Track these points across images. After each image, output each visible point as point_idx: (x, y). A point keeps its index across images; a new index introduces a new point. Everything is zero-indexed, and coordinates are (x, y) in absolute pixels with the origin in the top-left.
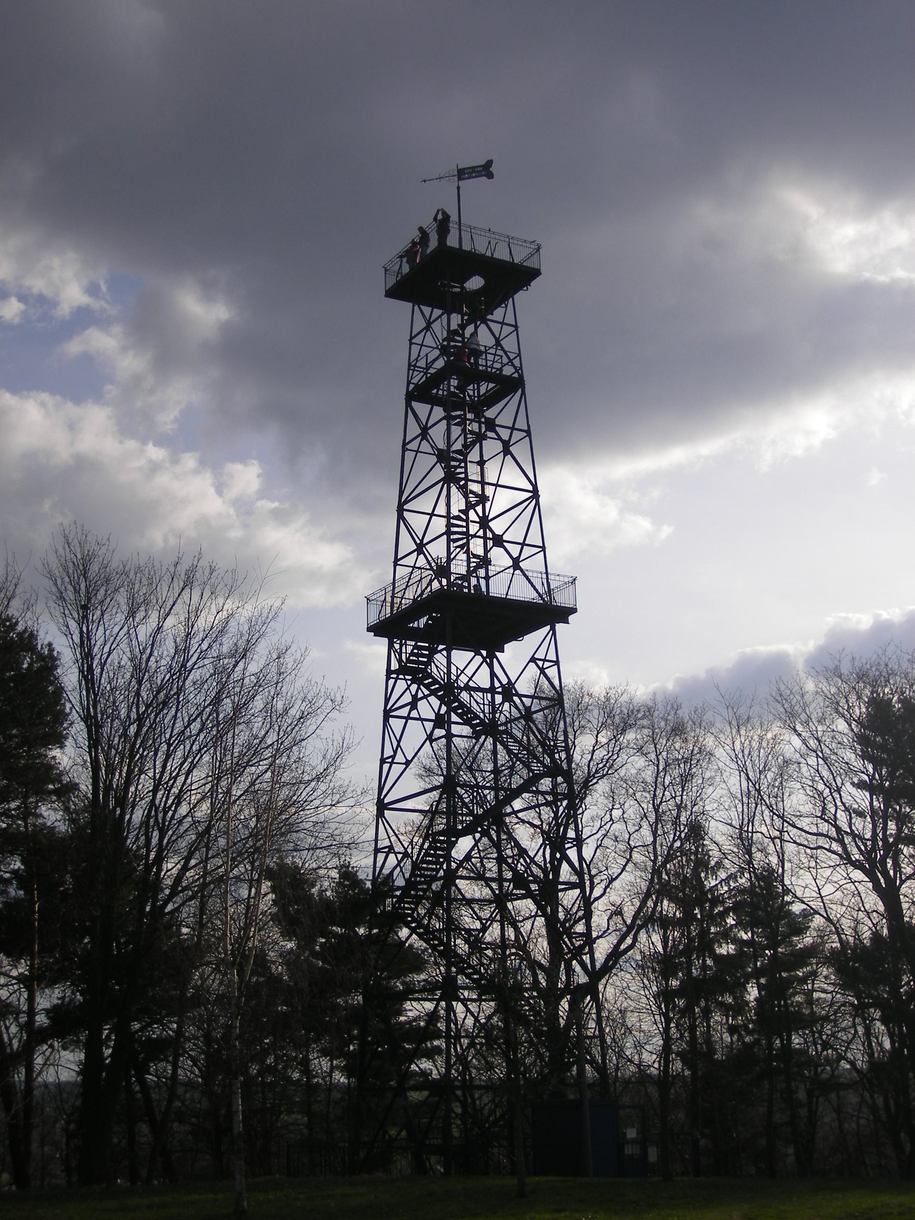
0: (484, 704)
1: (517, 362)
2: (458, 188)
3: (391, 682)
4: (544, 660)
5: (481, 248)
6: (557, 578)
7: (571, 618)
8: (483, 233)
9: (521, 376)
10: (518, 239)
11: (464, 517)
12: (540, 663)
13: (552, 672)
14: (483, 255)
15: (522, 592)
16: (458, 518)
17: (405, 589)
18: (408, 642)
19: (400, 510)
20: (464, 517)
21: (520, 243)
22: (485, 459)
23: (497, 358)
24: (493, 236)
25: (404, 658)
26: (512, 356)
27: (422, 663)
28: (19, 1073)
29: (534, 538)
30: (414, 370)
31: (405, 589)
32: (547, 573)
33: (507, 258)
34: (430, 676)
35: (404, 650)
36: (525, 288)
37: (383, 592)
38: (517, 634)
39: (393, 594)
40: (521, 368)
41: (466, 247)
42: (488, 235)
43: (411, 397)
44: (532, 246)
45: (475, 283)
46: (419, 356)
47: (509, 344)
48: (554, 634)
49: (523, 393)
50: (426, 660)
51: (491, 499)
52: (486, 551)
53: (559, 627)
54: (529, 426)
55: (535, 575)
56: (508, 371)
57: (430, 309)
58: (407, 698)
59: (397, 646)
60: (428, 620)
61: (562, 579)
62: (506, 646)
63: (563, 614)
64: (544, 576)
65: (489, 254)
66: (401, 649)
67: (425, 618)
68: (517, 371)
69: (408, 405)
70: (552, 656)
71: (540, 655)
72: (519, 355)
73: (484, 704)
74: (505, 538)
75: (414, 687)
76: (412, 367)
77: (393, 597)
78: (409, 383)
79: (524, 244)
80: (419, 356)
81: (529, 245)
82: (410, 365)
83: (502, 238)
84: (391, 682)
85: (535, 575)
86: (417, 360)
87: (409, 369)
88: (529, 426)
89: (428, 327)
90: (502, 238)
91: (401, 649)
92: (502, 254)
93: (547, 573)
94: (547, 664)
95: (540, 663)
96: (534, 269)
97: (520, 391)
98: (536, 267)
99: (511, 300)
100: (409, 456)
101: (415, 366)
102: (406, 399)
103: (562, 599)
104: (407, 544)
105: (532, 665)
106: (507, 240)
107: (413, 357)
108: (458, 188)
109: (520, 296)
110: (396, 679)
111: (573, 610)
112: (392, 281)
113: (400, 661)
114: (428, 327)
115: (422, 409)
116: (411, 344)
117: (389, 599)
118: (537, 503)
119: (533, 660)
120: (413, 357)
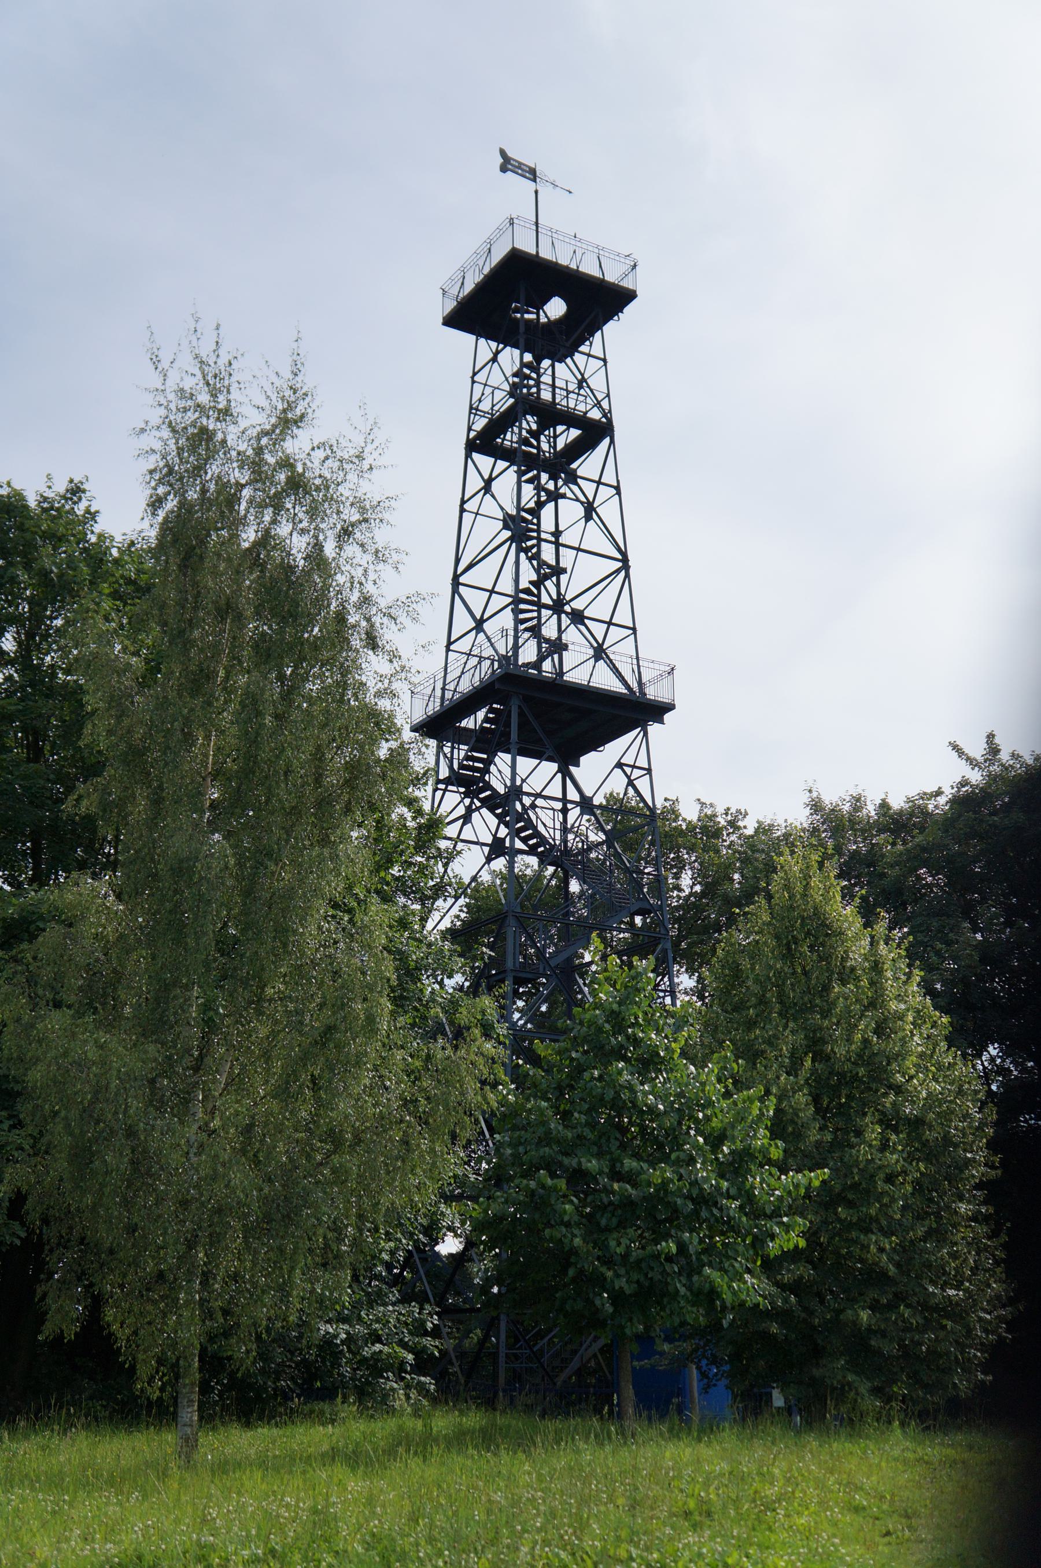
0: (554, 829)
1: (605, 404)
2: (536, 192)
3: (439, 794)
4: (633, 767)
5: (564, 259)
6: (651, 665)
7: (667, 717)
8: (567, 240)
9: (610, 421)
10: (611, 251)
11: (535, 591)
12: (628, 770)
13: (642, 784)
14: (567, 267)
15: (604, 680)
16: (527, 591)
17: (460, 677)
18: (461, 747)
19: (456, 582)
20: (535, 591)
21: (612, 256)
22: (561, 529)
23: (581, 398)
24: (579, 244)
25: (456, 766)
26: (600, 397)
27: (477, 770)
28: (684, 1285)
29: (623, 616)
30: (476, 414)
31: (460, 677)
32: (637, 658)
33: (595, 272)
34: (488, 786)
35: (456, 756)
36: (616, 318)
37: (432, 681)
38: (595, 743)
39: (445, 684)
40: (610, 411)
41: (546, 254)
42: (573, 242)
43: (472, 446)
44: (628, 262)
45: (556, 308)
46: (483, 394)
47: (597, 382)
48: (646, 734)
49: (612, 442)
50: (481, 766)
51: (569, 571)
52: (560, 631)
53: (653, 729)
54: (618, 481)
55: (624, 659)
56: (595, 414)
57: (493, 460)
58: (461, 811)
59: (447, 750)
60: (487, 713)
61: (657, 666)
62: (582, 759)
63: (658, 711)
64: (635, 662)
65: (573, 266)
66: (452, 753)
67: (484, 710)
68: (605, 415)
69: (468, 456)
70: (642, 762)
71: (628, 759)
72: (608, 395)
73: (554, 829)
74: (586, 613)
75: (467, 801)
76: (473, 410)
77: (443, 689)
78: (470, 429)
79: (617, 258)
80: (483, 394)
81: (623, 260)
82: (471, 408)
83: (591, 248)
84: (439, 794)
85: (624, 659)
86: (480, 401)
87: (470, 413)
88: (618, 481)
89: (487, 487)
90: (591, 248)
91: (452, 753)
92: (589, 268)
93: (637, 658)
94: (637, 773)
95: (628, 770)
96: (627, 289)
97: (608, 439)
98: (631, 287)
99: (598, 334)
100: (468, 518)
101: (477, 409)
102: (466, 449)
103: (653, 693)
104: (463, 622)
105: (618, 771)
106: (596, 251)
107: (475, 398)
108: (536, 192)
109: (609, 327)
110: (445, 790)
111: (669, 707)
112: (451, 305)
113: (451, 767)
114: (487, 487)
115: (484, 462)
116: (473, 382)
117: (438, 693)
118: (627, 576)
119: (620, 765)
120: (475, 398)
